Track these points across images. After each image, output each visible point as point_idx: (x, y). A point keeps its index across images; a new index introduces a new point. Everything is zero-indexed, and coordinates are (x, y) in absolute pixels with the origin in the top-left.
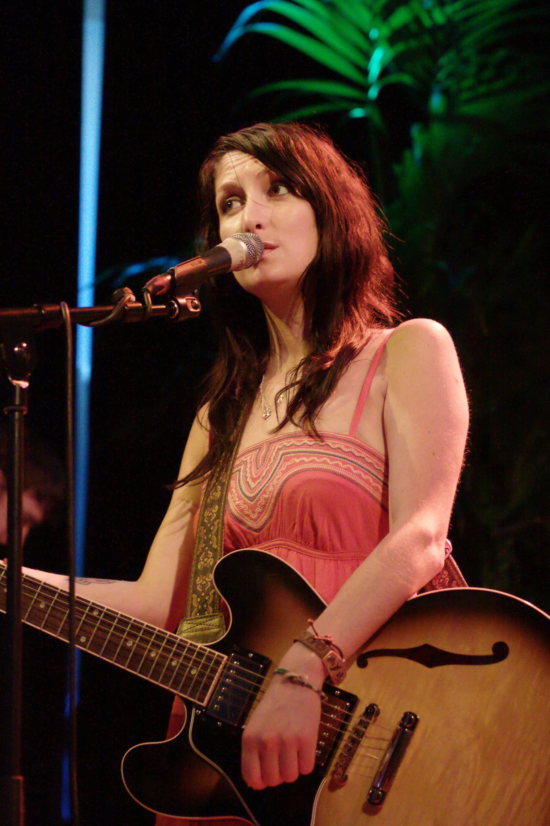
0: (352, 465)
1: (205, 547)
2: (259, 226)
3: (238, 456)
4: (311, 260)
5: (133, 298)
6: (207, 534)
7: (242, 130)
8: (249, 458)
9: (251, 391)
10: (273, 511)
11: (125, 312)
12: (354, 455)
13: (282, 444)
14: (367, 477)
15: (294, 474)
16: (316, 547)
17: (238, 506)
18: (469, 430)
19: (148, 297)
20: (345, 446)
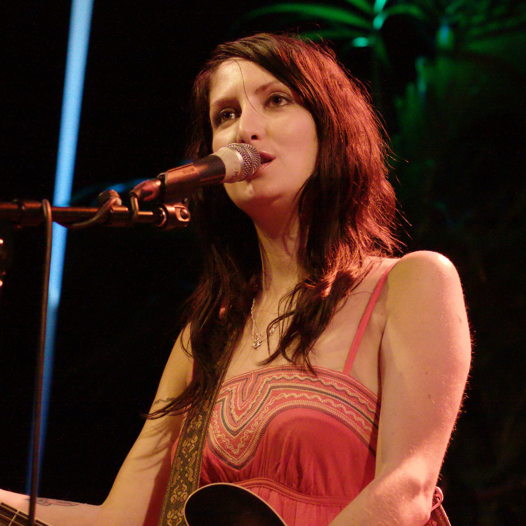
0: (344, 405)
1: (180, 479)
2: (255, 137)
3: (223, 384)
4: (309, 175)
5: (119, 202)
6: (183, 466)
7: (246, 39)
8: (234, 388)
9: (240, 317)
10: (256, 448)
11: (110, 216)
12: (347, 394)
13: (271, 376)
14: (359, 419)
15: (281, 411)
16: (299, 491)
17: (219, 439)
18: (469, 374)
19: (135, 202)
20: (338, 383)
